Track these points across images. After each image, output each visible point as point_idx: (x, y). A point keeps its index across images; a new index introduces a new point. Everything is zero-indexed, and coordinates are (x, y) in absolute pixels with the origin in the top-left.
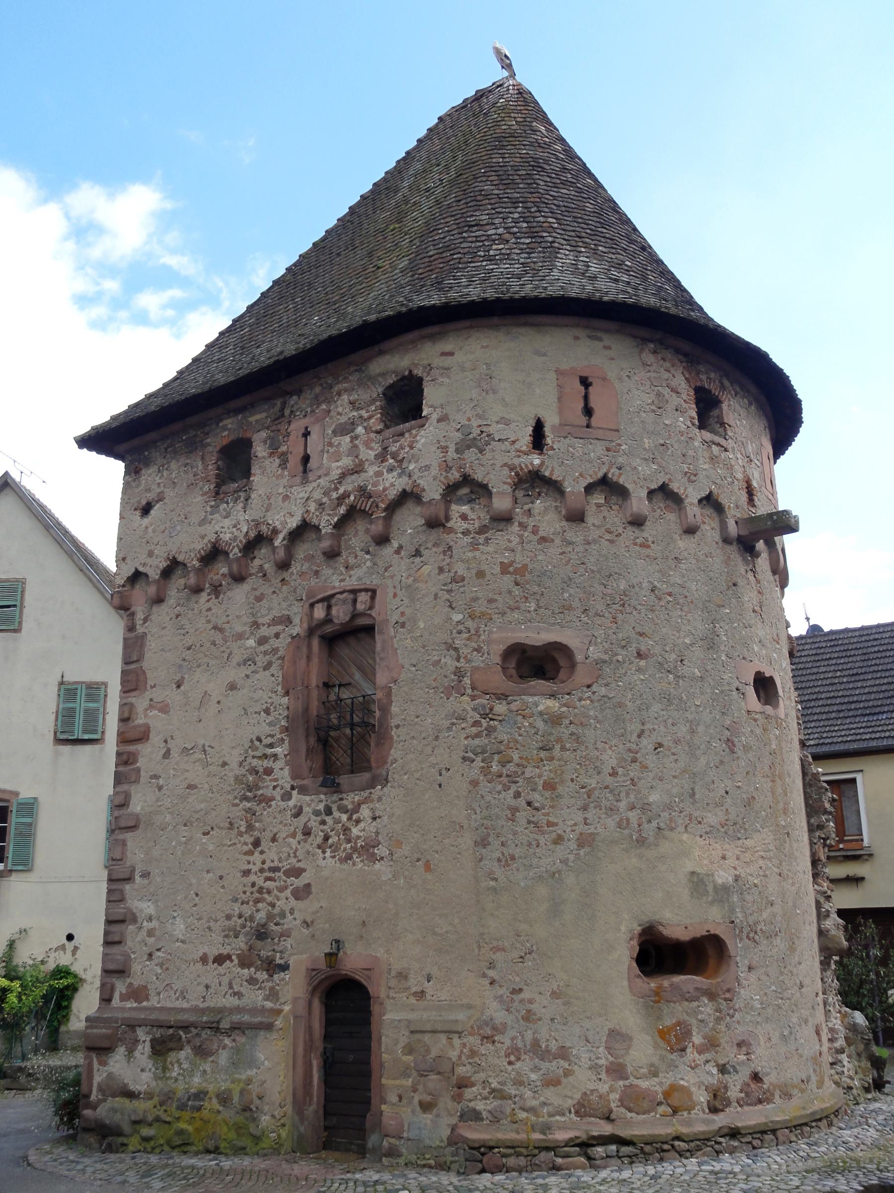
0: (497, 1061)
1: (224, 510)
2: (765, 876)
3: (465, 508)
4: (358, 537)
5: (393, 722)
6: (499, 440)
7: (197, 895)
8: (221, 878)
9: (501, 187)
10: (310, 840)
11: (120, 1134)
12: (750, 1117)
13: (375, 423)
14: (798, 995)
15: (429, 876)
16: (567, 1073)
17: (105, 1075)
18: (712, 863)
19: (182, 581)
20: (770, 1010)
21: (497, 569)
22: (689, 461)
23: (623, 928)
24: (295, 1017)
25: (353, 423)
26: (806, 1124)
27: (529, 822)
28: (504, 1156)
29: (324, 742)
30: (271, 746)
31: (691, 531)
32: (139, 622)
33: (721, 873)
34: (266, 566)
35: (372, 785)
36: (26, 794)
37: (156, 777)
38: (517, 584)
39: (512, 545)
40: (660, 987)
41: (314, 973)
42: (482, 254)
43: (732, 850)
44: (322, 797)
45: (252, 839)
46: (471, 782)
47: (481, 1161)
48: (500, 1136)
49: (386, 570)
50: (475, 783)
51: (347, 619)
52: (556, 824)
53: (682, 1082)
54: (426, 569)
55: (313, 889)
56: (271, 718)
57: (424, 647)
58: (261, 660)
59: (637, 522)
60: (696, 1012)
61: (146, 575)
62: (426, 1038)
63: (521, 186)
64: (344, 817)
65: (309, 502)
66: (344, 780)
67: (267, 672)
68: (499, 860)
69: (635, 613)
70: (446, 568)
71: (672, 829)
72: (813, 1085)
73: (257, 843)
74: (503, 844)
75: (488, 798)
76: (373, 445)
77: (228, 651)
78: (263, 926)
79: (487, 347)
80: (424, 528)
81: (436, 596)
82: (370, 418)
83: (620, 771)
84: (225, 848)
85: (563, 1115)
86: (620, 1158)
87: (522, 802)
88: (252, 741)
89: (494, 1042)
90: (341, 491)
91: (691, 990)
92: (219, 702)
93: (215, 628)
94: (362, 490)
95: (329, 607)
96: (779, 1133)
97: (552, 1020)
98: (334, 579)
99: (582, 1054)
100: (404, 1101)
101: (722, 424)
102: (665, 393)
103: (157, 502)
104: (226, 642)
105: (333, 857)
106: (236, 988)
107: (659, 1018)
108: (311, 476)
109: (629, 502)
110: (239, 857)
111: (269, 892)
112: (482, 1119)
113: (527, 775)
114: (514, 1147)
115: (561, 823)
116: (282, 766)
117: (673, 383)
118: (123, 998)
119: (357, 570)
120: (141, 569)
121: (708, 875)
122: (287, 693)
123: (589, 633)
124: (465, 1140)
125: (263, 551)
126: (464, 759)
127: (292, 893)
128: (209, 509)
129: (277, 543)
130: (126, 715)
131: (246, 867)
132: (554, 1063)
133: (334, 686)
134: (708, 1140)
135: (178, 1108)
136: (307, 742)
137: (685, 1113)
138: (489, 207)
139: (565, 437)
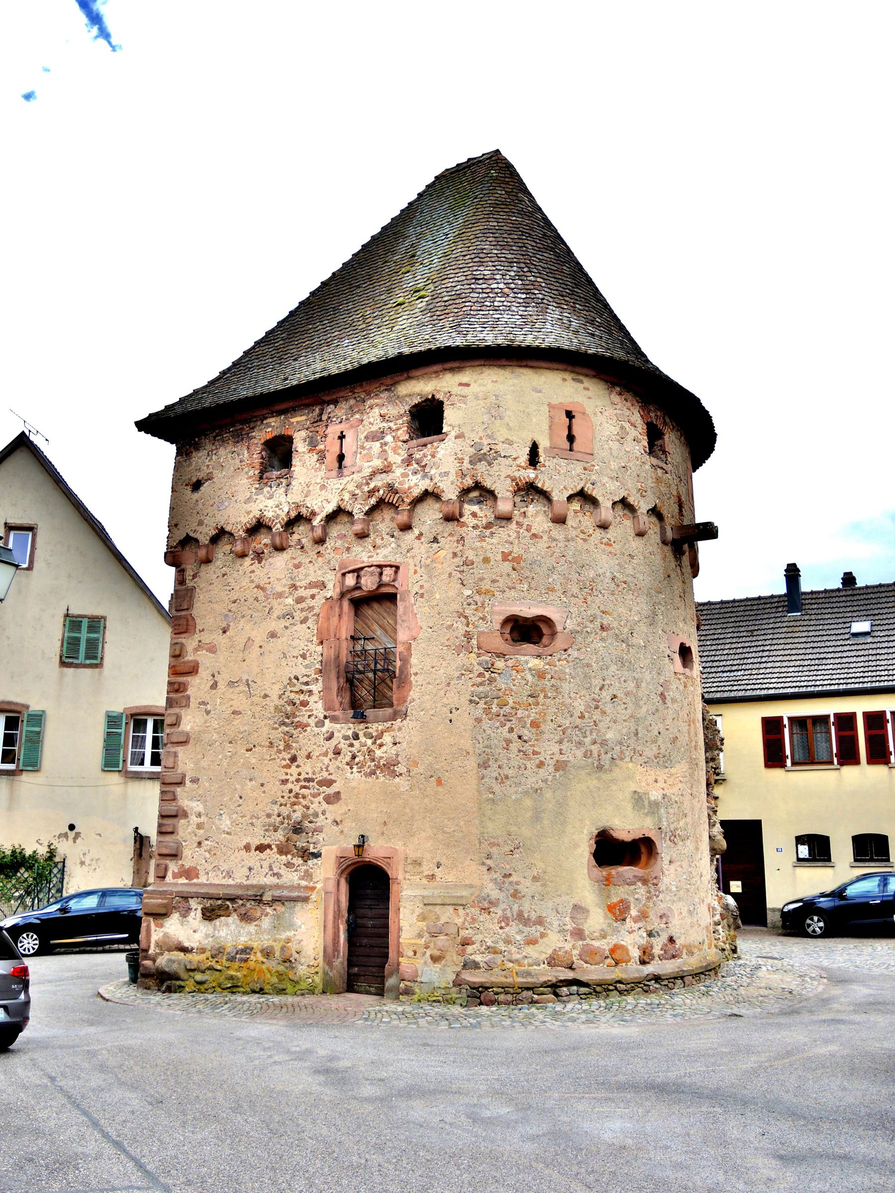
0: (491, 926)
1: (268, 492)
2: (682, 795)
3: (475, 508)
4: (385, 522)
5: (413, 670)
6: (504, 457)
7: (241, 797)
8: (262, 785)
9: (498, 247)
10: (340, 758)
11: (178, 978)
12: (667, 967)
13: (403, 434)
14: (699, 882)
15: (440, 789)
16: (543, 935)
17: (162, 934)
18: (648, 785)
19: (228, 547)
20: (682, 892)
21: (499, 557)
22: (642, 480)
23: (585, 831)
24: (326, 893)
25: (383, 432)
26: (702, 973)
27: (519, 751)
28: (497, 994)
29: (350, 681)
30: (307, 683)
31: (640, 534)
32: (188, 578)
33: (654, 793)
34: (304, 541)
35: (394, 718)
36: (35, 706)
37: (203, 703)
38: (514, 569)
39: (511, 539)
40: (609, 874)
41: (343, 860)
42: (489, 304)
43: (662, 775)
44: (351, 725)
45: (289, 756)
46: (476, 719)
47: (479, 998)
48: (493, 979)
49: (408, 551)
50: (479, 720)
51: (374, 587)
52: (540, 753)
53: (622, 943)
54: (442, 553)
55: (342, 796)
56: (307, 662)
57: (439, 613)
58: (299, 616)
59: (604, 526)
60: (634, 892)
61: (197, 540)
62: (437, 908)
63: (514, 248)
64: (369, 742)
65: (344, 492)
66: (370, 713)
67: (304, 625)
68: (496, 779)
69: (600, 595)
70: (459, 554)
71: (622, 759)
72: (706, 946)
73: (293, 759)
74: (499, 767)
75: (488, 732)
76: (400, 451)
77: (269, 606)
78: (299, 823)
79: (496, 382)
80: (441, 521)
81: (450, 574)
82: (398, 429)
83: (587, 715)
84: (266, 762)
85: (539, 965)
86: (579, 995)
87: (514, 736)
88: (290, 679)
89: (489, 912)
90: (372, 486)
91: (631, 877)
92: (261, 647)
93: (258, 587)
94: (391, 488)
95: (358, 577)
96: (686, 979)
97: (533, 897)
98: (362, 555)
99: (554, 921)
100: (418, 955)
101: (664, 452)
102: (627, 427)
103: (206, 480)
104: (268, 599)
105: (360, 772)
106: (276, 870)
107: (608, 897)
108: (345, 471)
109: (598, 510)
110: (278, 769)
111: (304, 797)
112: (480, 968)
113: (519, 716)
114: (505, 988)
115: (543, 753)
116: (317, 699)
117: (632, 420)
118: (175, 876)
119: (383, 548)
120: (192, 534)
121: (645, 794)
122: (322, 643)
123: (566, 610)
124: (468, 983)
125: (301, 528)
126: (471, 701)
127: (324, 799)
128: (254, 491)
129: (316, 522)
130: (177, 653)
131: (284, 777)
132: (534, 928)
133: (360, 639)
134: (640, 983)
135: (228, 960)
136: (338, 682)
137: (624, 964)
138: (490, 264)
139: (554, 458)
